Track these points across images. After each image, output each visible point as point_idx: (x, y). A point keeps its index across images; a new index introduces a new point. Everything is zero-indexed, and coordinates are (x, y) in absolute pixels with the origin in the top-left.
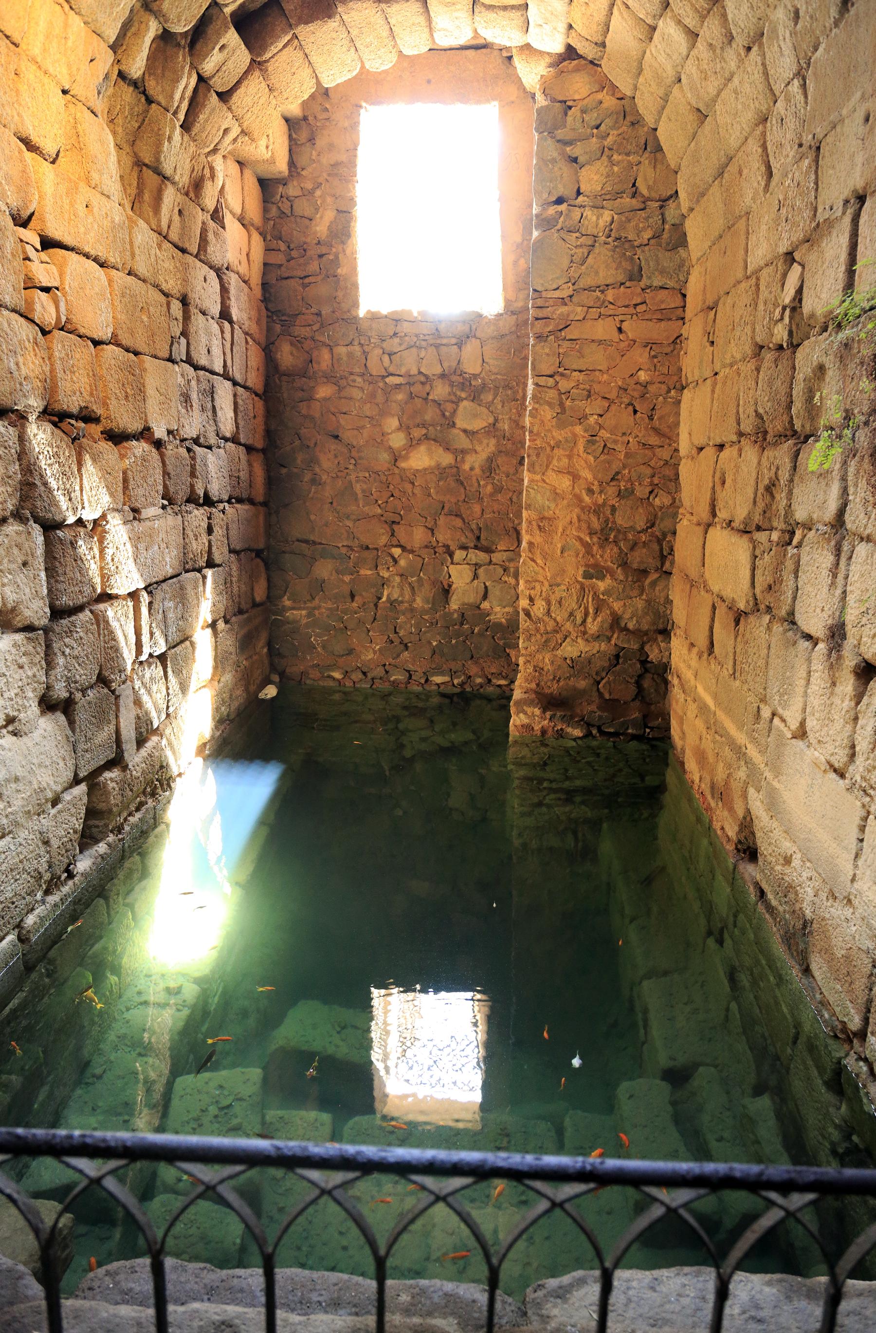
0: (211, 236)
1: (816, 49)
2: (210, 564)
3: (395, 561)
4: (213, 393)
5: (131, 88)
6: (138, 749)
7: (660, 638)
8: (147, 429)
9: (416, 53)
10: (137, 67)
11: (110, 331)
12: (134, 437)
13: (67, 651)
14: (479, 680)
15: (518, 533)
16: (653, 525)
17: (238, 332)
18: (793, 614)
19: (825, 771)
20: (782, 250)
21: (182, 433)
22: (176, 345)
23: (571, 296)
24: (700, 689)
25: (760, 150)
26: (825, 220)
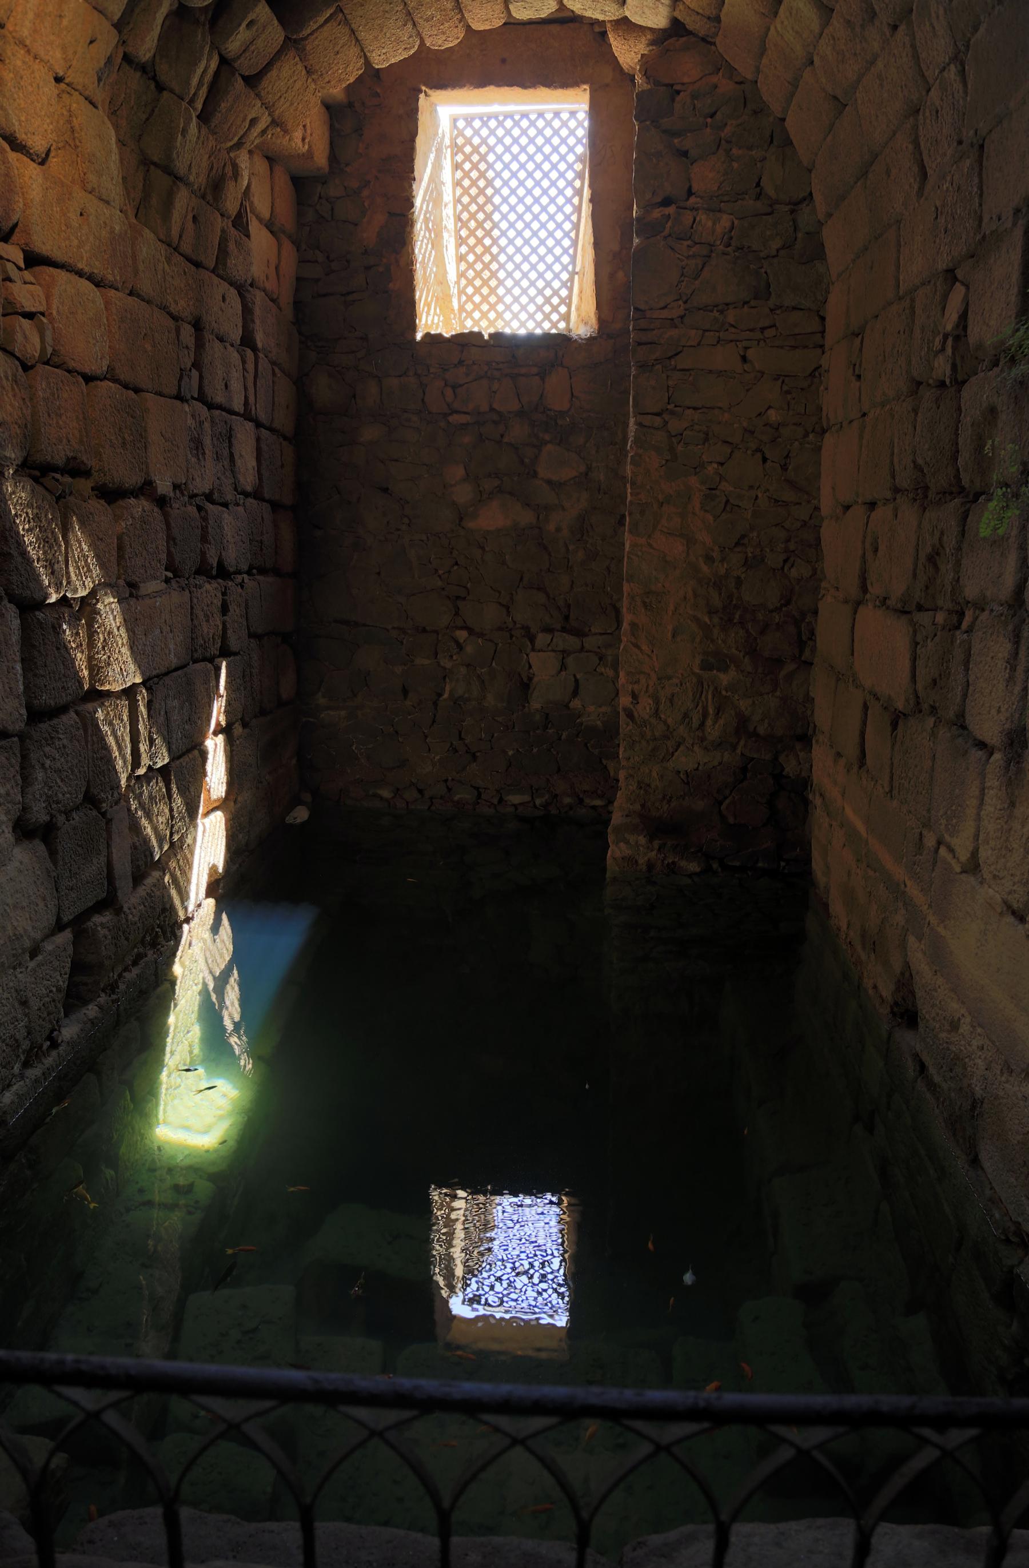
0: (232, 246)
1: (976, 29)
2: (225, 652)
3: (460, 647)
4: (230, 437)
5: (138, 74)
6: (135, 887)
7: (798, 746)
8: (149, 483)
9: (487, 27)
10: (146, 48)
11: (105, 363)
12: (132, 493)
13: (48, 762)
14: (567, 800)
15: (617, 611)
16: (788, 603)
17: (263, 362)
18: (963, 716)
19: (1001, 914)
20: (941, 266)
21: (191, 487)
22: (186, 379)
23: (682, 317)
24: (849, 811)
25: (911, 147)
26: (992, 232)
